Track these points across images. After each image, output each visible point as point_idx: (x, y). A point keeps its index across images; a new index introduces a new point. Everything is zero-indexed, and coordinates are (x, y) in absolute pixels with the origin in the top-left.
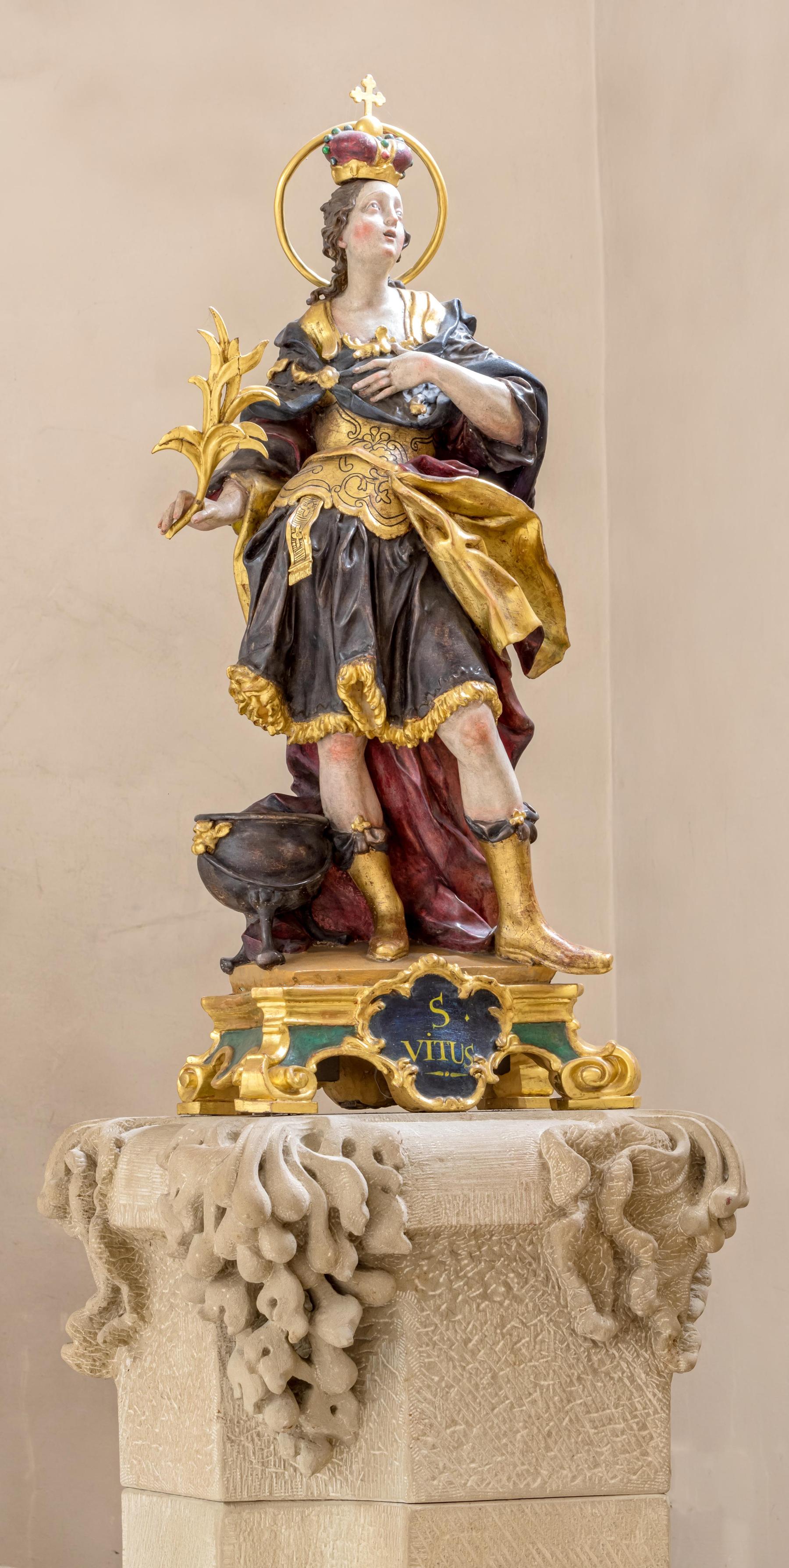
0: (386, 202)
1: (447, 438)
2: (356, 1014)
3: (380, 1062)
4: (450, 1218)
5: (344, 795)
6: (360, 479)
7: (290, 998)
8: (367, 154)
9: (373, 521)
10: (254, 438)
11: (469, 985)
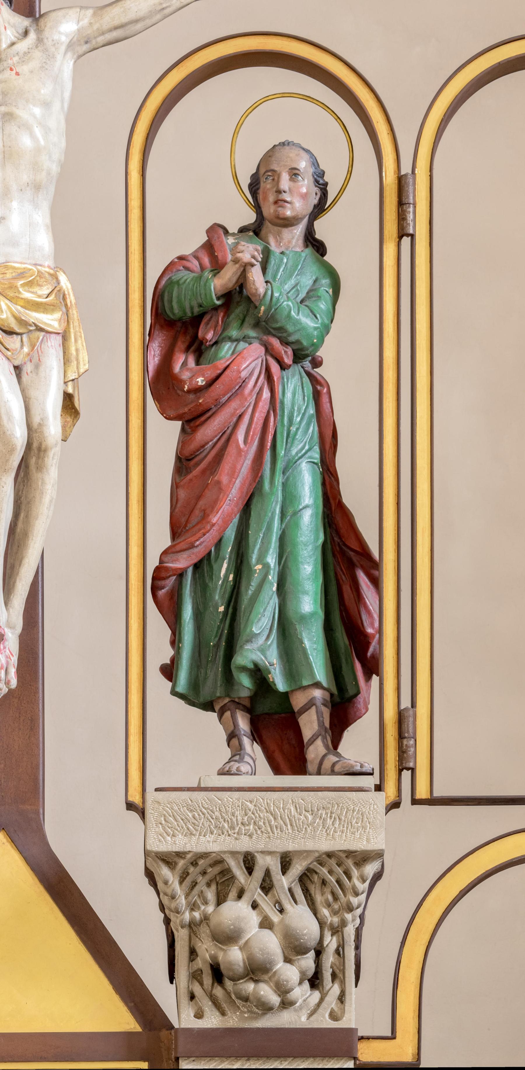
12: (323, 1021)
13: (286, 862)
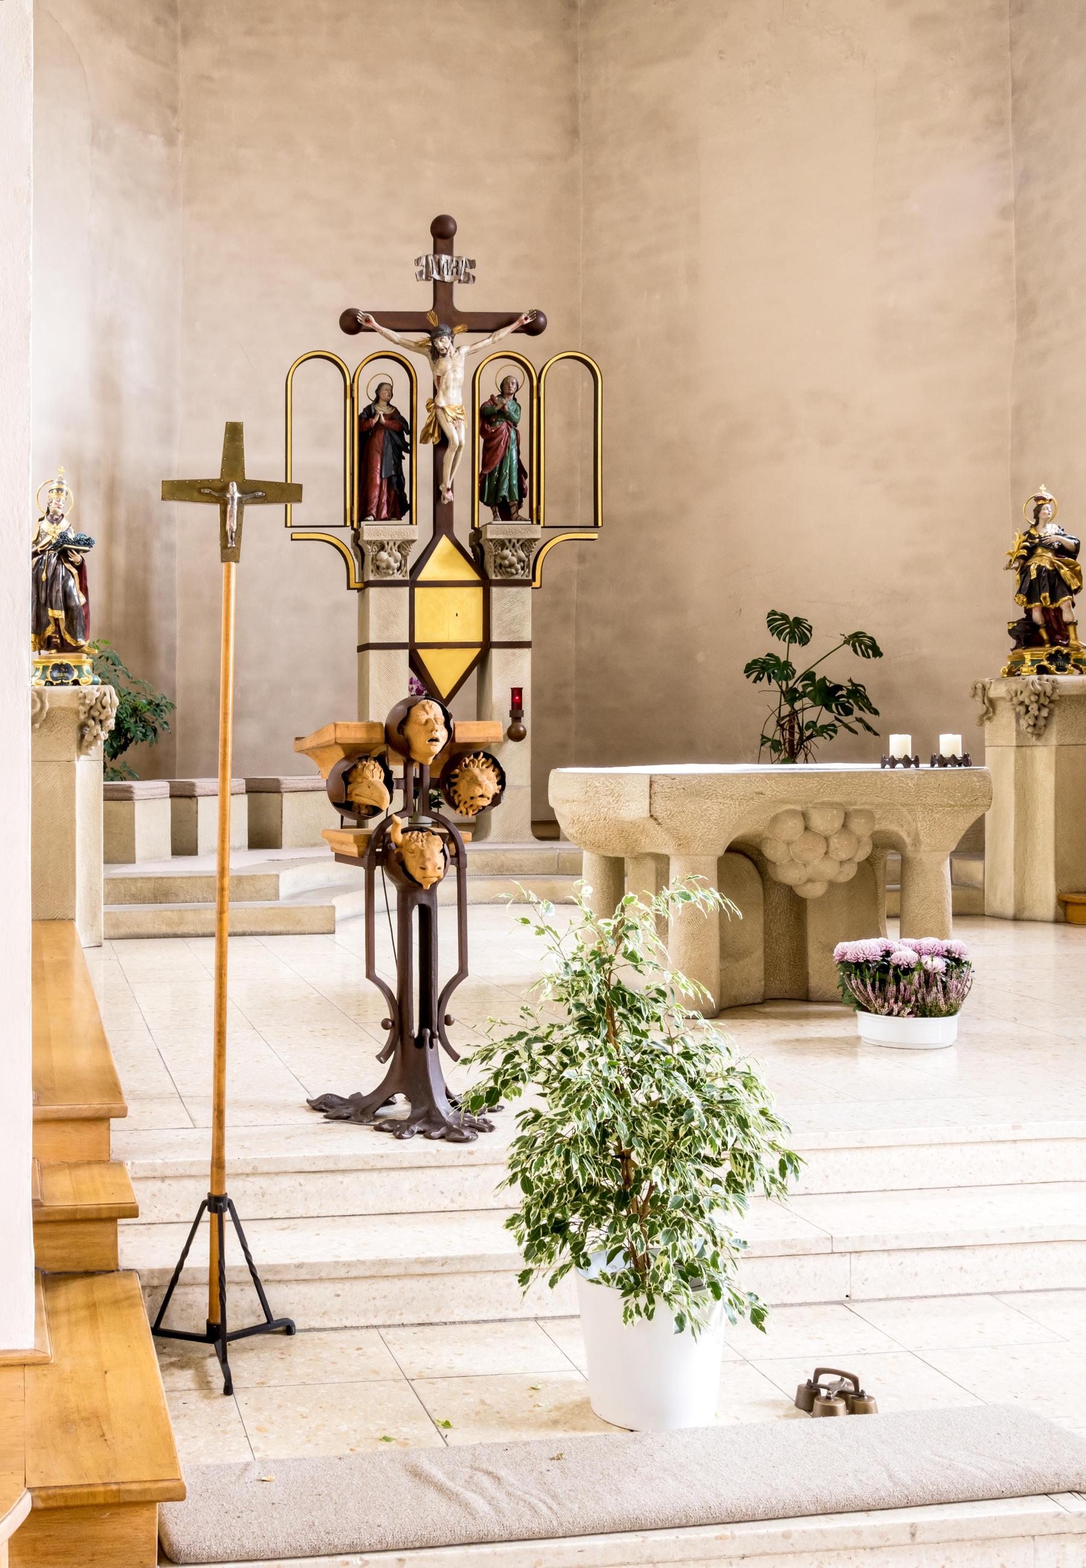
0: (1047, 509)
1: (1061, 551)
2: (1044, 658)
3: (1049, 666)
4: (1066, 693)
5: (1037, 616)
6: (1044, 560)
7: (1032, 655)
8: (1044, 499)
9: (1048, 567)
10: (1024, 552)
11: (1065, 651)
12: (524, 578)
13: (518, 541)
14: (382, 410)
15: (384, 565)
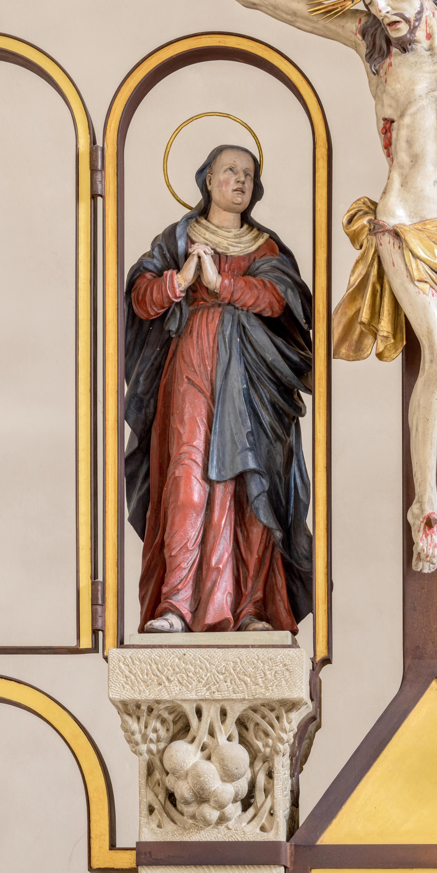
14: (223, 236)
15: (183, 789)
